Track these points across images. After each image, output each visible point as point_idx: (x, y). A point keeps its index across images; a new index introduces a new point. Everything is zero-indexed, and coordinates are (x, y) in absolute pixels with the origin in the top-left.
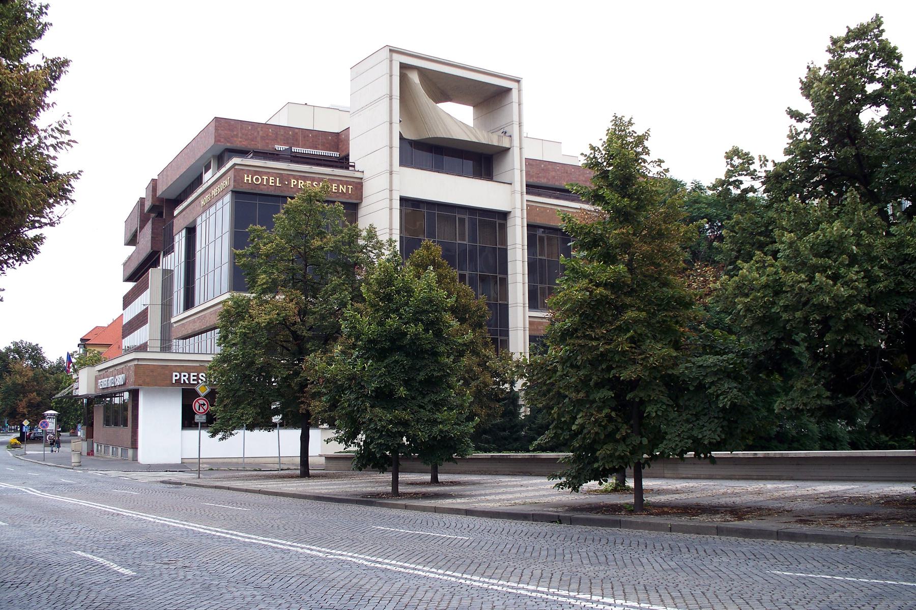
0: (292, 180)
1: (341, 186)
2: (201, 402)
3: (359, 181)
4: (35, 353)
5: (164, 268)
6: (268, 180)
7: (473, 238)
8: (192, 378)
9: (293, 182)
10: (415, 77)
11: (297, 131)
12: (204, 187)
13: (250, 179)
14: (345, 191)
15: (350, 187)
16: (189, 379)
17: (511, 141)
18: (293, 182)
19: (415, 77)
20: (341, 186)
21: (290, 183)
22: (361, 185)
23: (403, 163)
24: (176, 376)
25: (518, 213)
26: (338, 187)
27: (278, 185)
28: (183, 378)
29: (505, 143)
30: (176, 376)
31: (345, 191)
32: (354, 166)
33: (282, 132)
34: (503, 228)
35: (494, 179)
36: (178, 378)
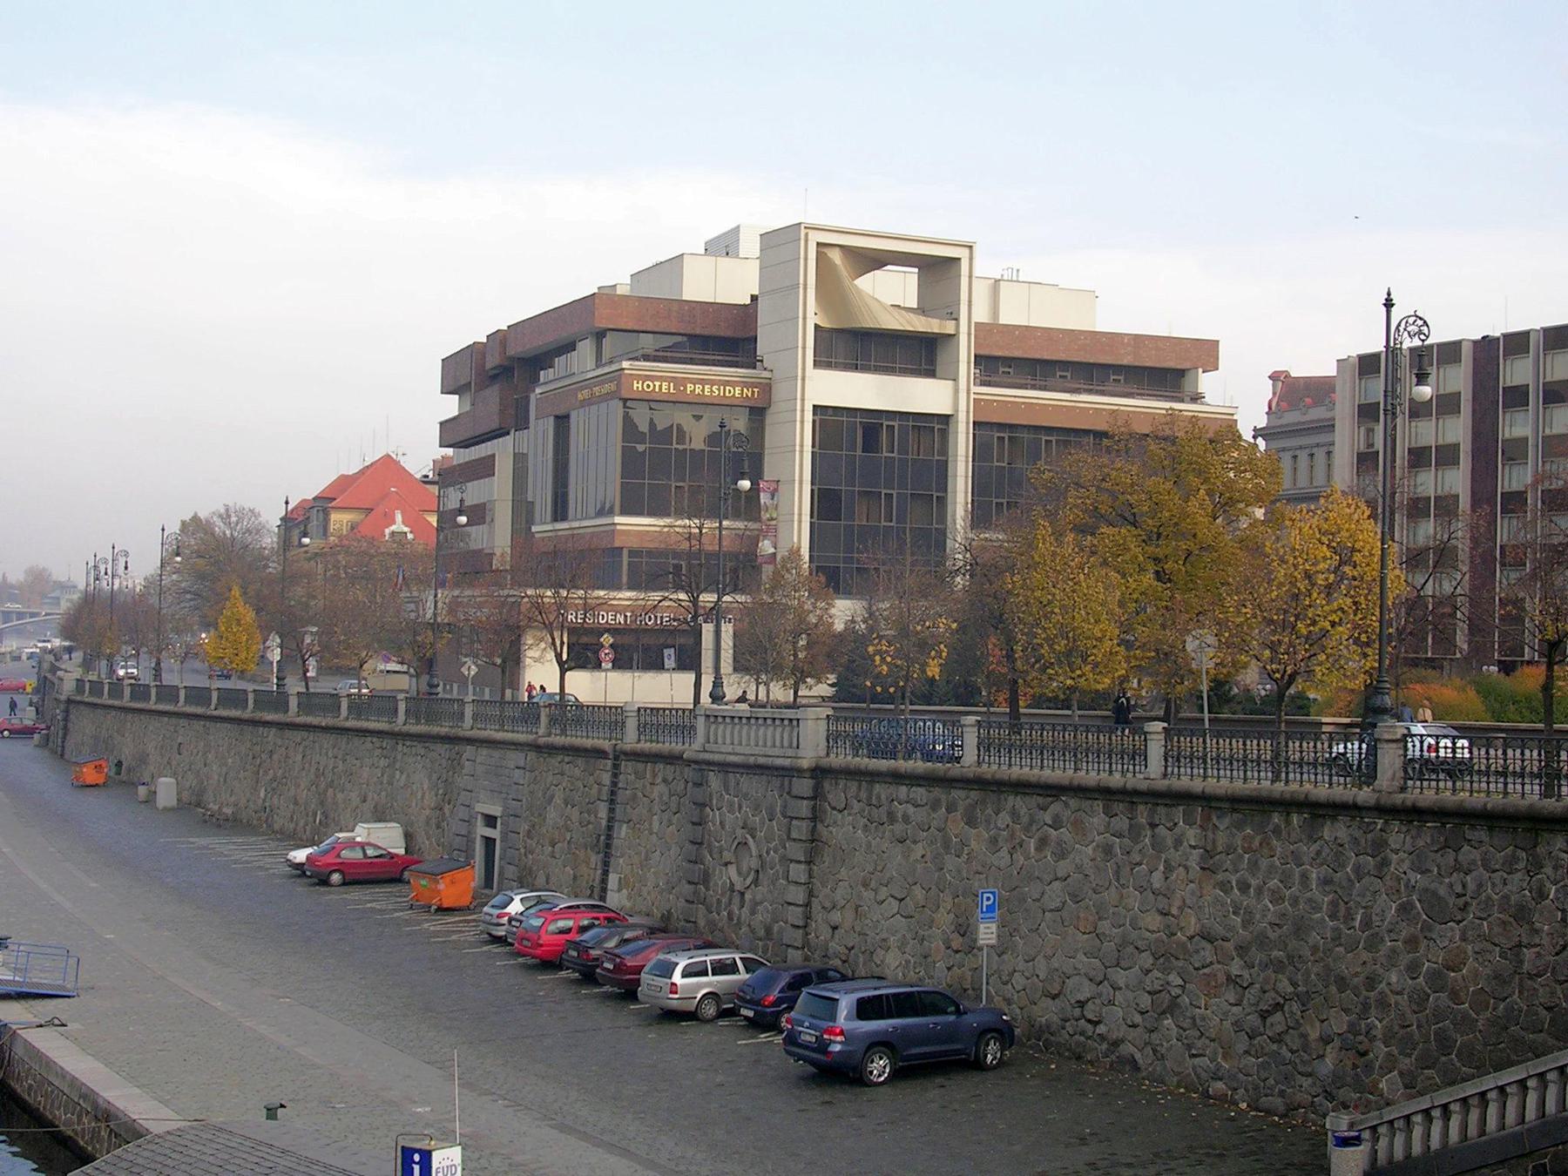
0: (689, 385)
1: (745, 390)
2: (607, 651)
3: (768, 381)
4: (256, 515)
5: (517, 451)
6: (660, 386)
7: (903, 450)
8: (579, 616)
9: (690, 387)
10: (836, 257)
11: (694, 305)
12: (792, 972)
13: (640, 385)
14: (750, 395)
15: (756, 390)
16: (576, 618)
17: (958, 326)
18: (690, 387)
19: (836, 257)
20: (745, 390)
21: (686, 388)
22: (770, 386)
23: (817, 364)
24: (988, 899)
25: (962, 417)
26: (742, 390)
27: (672, 391)
28: (570, 617)
29: (949, 328)
30: (988, 899)
31: (750, 395)
32: (762, 361)
33: (675, 307)
34: (944, 434)
35: (938, 374)
36: (990, 903)
